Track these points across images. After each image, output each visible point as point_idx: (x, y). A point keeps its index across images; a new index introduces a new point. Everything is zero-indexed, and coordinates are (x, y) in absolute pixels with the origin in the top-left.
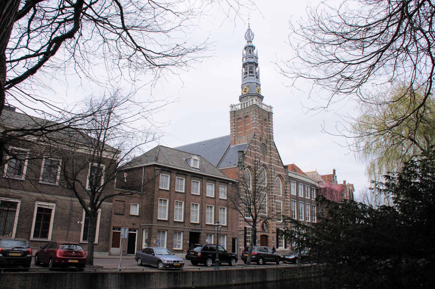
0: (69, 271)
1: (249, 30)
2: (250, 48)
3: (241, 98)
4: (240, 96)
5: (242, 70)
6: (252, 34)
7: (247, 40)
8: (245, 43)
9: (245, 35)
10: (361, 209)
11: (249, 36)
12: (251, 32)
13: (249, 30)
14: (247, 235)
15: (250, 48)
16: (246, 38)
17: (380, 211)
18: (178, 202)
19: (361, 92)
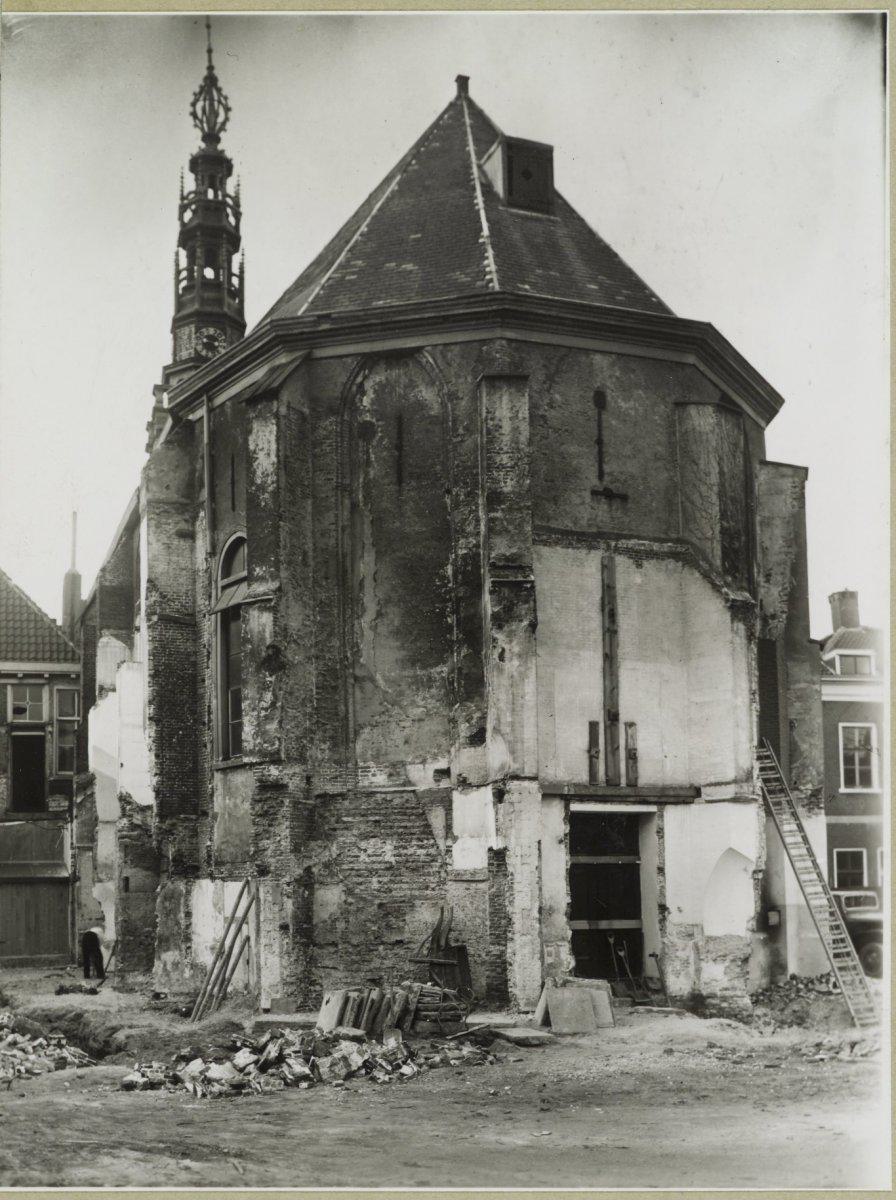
2: (212, 166)
15: (212, 166)
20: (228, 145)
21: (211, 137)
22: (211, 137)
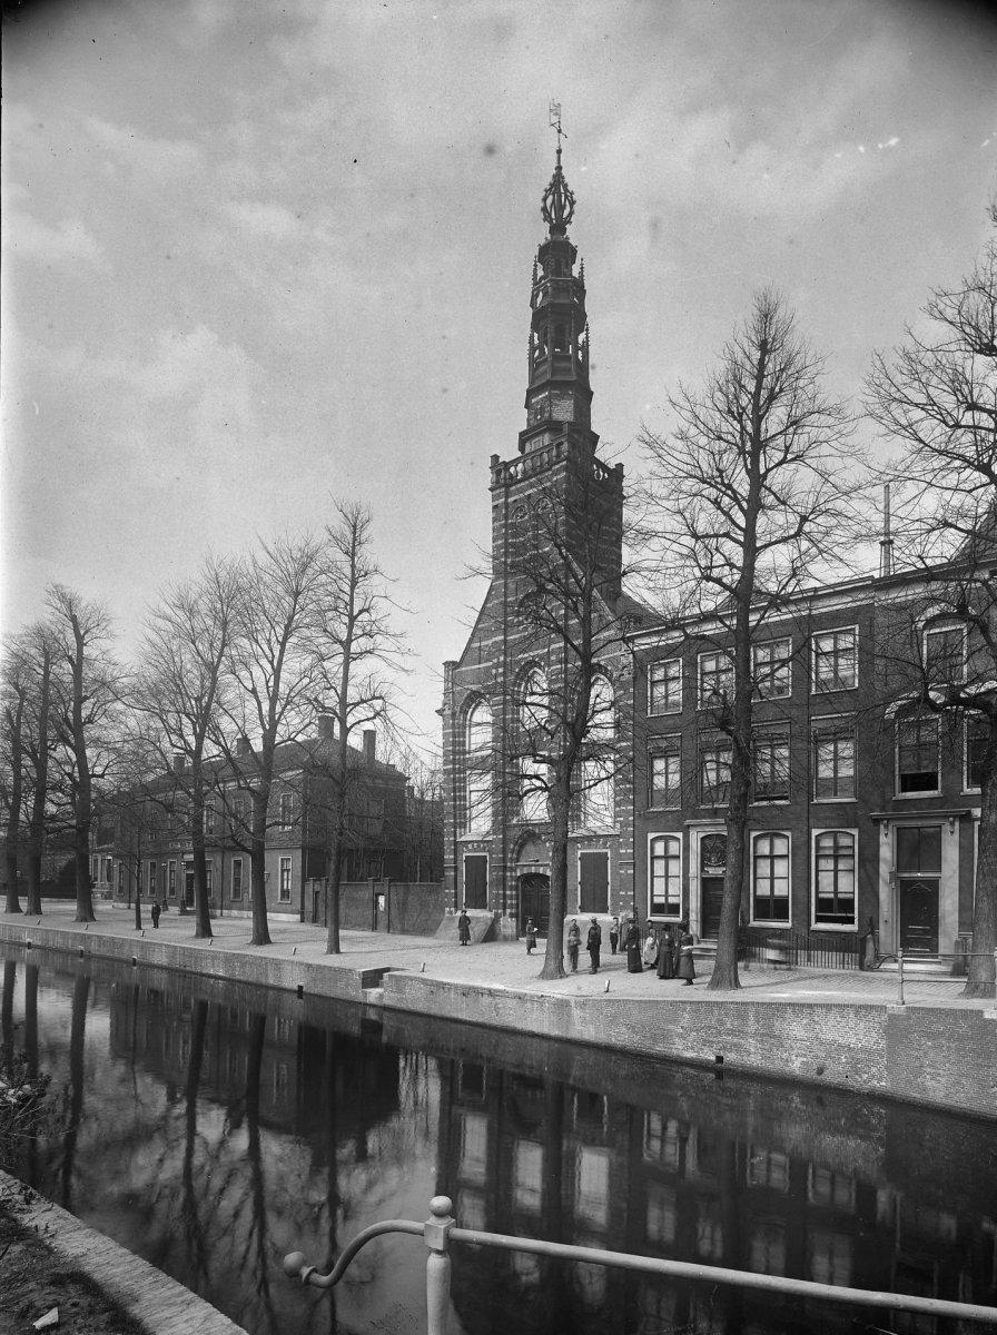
0: (853, 912)
1: (558, 180)
2: (557, 255)
3: (524, 438)
4: (521, 434)
5: (532, 337)
6: (566, 197)
7: (550, 221)
8: (543, 233)
9: (545, 200)
10: (651, 935)
11: (558, 201)
12: (566, 186)
13: (558, 180)
14: (501, 856)
15: (557, 255)
16: (547, 218)
17: (94, 795)
18: (517, 908)
19: (968, 489)
22: (558, 227)
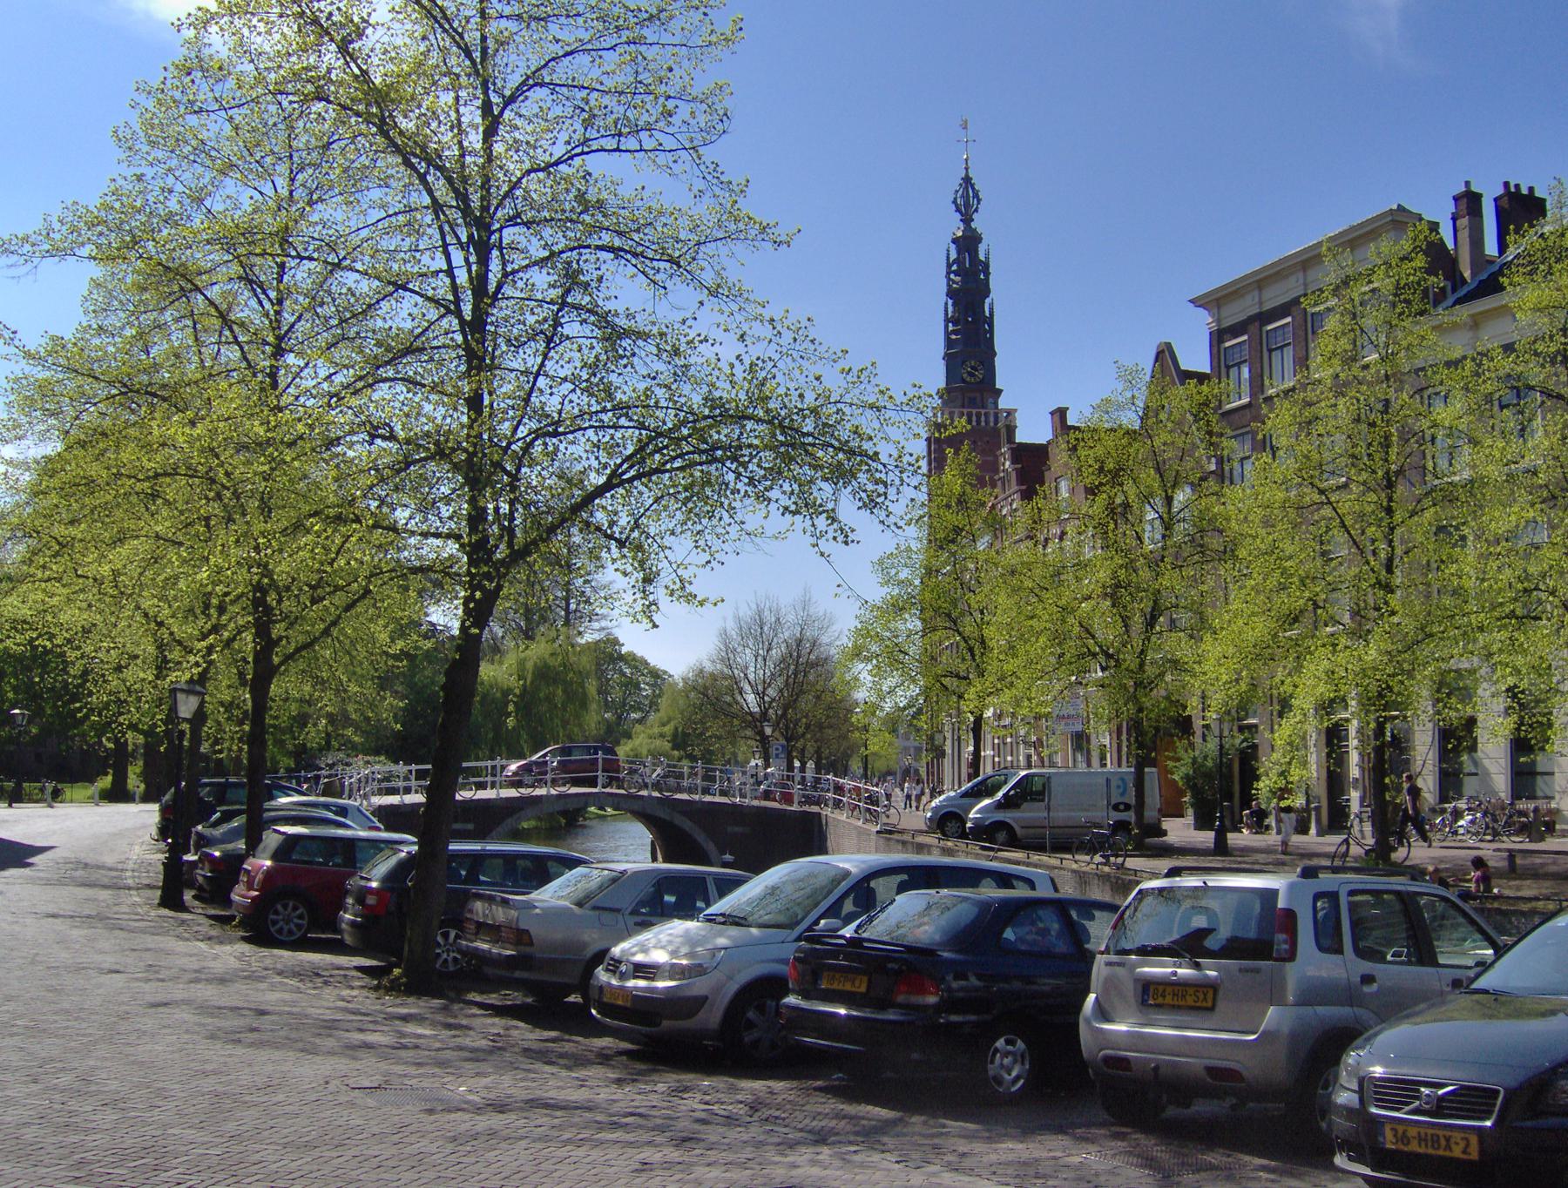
2: (968, 243)
15: (968, 243)
20: (978, 224)
21: (967, 220)
22: (967, 220)
